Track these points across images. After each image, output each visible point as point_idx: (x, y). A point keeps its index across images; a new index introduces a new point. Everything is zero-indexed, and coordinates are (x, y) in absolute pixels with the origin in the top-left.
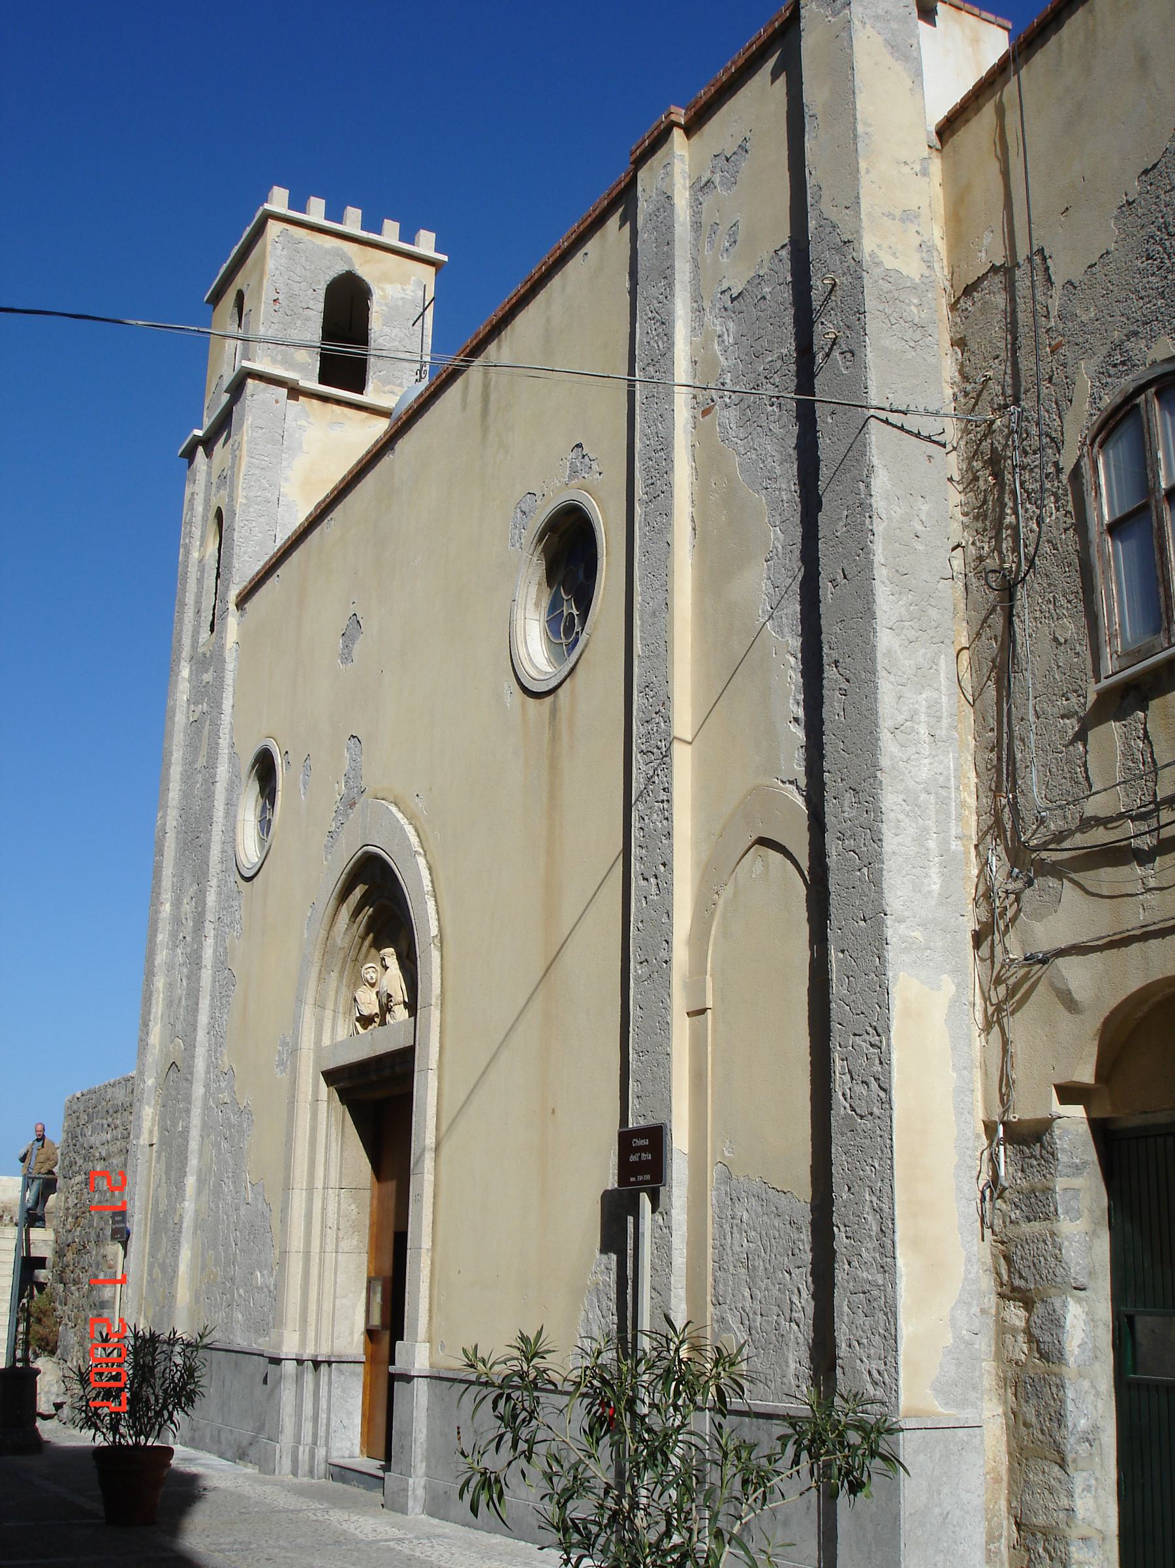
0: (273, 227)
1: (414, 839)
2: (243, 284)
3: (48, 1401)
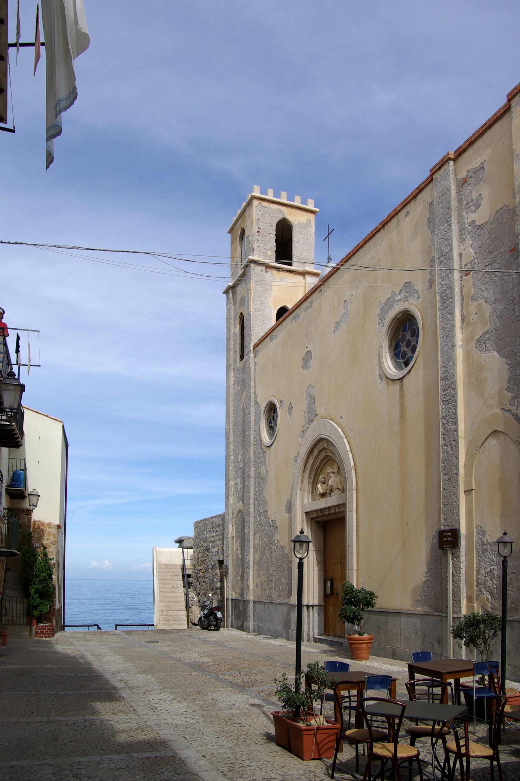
0: (256, 203)
1: (341, 433)
2: (244, 225)
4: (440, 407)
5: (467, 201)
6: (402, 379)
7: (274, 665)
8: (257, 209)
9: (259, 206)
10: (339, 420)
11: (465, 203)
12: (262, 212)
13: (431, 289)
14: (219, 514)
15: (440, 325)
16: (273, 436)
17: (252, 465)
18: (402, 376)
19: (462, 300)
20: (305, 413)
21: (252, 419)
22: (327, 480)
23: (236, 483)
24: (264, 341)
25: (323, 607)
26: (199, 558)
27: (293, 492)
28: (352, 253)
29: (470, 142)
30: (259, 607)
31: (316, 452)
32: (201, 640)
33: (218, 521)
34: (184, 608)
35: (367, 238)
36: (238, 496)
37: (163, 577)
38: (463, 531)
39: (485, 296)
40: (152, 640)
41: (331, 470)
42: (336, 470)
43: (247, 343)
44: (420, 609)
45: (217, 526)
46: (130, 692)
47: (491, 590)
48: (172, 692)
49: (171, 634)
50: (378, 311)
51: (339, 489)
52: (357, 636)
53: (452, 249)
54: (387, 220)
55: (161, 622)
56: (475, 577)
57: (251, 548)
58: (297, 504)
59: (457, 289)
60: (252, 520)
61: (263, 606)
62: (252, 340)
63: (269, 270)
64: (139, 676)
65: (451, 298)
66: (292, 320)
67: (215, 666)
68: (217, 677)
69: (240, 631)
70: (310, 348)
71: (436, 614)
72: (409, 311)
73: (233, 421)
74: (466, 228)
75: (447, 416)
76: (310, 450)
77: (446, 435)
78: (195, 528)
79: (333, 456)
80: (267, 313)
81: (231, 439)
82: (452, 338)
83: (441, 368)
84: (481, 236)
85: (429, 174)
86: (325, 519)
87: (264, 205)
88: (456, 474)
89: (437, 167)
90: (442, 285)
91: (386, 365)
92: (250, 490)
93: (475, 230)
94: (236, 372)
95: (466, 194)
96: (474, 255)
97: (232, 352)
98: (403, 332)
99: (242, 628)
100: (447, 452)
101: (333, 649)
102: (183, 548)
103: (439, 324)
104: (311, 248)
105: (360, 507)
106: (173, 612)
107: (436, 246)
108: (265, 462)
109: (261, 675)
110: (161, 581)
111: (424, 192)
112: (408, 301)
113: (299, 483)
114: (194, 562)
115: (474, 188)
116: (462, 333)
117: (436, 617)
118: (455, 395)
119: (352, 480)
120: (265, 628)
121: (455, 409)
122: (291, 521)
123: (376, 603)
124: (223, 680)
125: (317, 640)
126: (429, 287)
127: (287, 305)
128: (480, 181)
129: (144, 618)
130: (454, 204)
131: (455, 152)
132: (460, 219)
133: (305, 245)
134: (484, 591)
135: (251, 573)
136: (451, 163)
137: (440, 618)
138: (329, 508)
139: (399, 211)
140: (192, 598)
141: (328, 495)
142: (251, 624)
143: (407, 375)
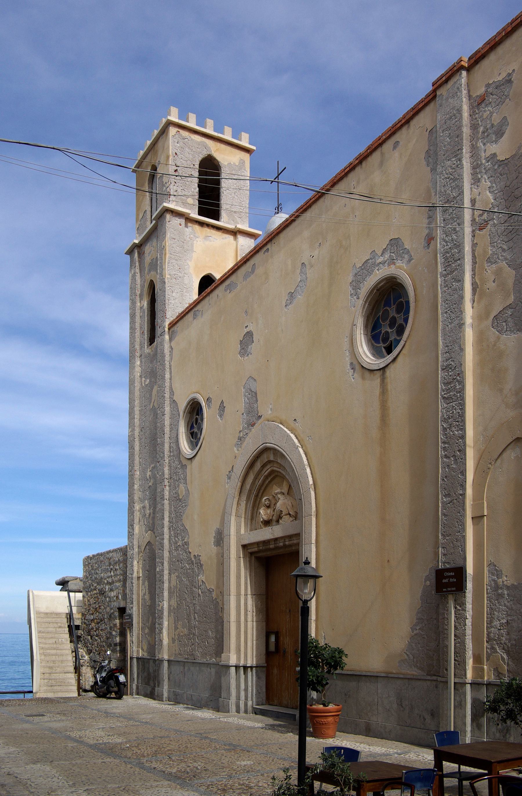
0: (172, 131)
1: (296, 441)
3: (89, 684)
4: (440, 406)
5: (485, 127)
6: (384, 369)
7: (213, 746)
8: (175, 140)
9: (177, 136)
10: (292, 424)
11: (481, 129)
12: (181, 144)
13: (428, 248)
14: (118, 547)
15: (442, 297)
16: (197, 446)
17: (166, 482)
18: (384, 365)
19: (474, 263)
20: (243, 414)
21: (167, 422)
22: (273, 502)
23: (144, 507)
24: (184, 318)
25: (265, 669)
26: (90, 605)
27: (226, 518)
28: (313, 199)
29: (493, 43)
30: (177, 669)
31: (258, 465)
32: (101, 712)
33: (117, 557)
34: (72, 669)
35: (337, 179)
36: (146, 524)
37: (43, 630)
38: (470, 570)
39: (508, 257)
40: (35, 714)
41: (278, 490)
42: (285, 490)
43: (159, 321)
44: (414, 672)
45: (116, 563)
46: (27, 792)
47: (508, 647)
48: (87, 790)
49: (57, 704)
50: (350, 278)
51: (290, 514)
52: (321, 706)
53: (463, 192)
54: (366, 154)
55: (41, 689)
56: (485, 631)
57: (165, 591)
58: (231, 534)
59: (467, 248)
60: (166, 554)
61: (182, 668)
62: (168, 316)
63: (189, 224)
64: (32, 766)
65: (459, 259)
66: (226, 290)
67: (133, 749)
68: (141, 766)
69: (150, 699)
70: (251, 328)
71: (429, 678)
72: (395, 278)
73: (140, 425)
74: (482, 164)
75: (450, 418)
76: (250, 463)
77: (448, 443)
78: (85, 565)
79: (282, 472)
80: (186, 282)
81: (137, 448)
82: (459, 313)
83: (443, 354)
84: (505, 176)
85: (431, 88)
86: (269, 554)
87: (183, 135)
88: (461, 495)
89: (444, 78)
90: (446, 242)
91: (361, 350)
92: (163, 516)
93: (496, 167)
94: (143, 360)
95: (485, 117)
96: (493, 201)
97: (138, 334)
98: (384, 306)
99: (152, 695)
100: (448, 466)
101: (282, 723)
102: (69, 591)
103: (440, 295)
104: (245, 199)
105: (321, 538)
106: (58, 674)
107: (438, 189)
108: (185, 479)
109: (201, 761)
110: (41, 634)
111: (422, 115)
112: (394, 264)
113: (233, 506)
114: (83, 610)
115: (496, 110)
116: (473, 308)
117: (429, 683)
118: (462, 390)
119: (311, 503)
120: (185, 695)
121: (460, 409)
122: (222, 556)
123: (346, 664)
124: (151, 769)
125: (256, 712)
126: (426, 245)
127: (212, 273)
128: (505, 99)
129: (22, 684)
130: (466, 131)
131: (470, 59)
132: (473, 152)
133: (236, 194)
134: (498, 649)
135: (166, 624)
136: (464, 73)
137: (434, 683)
138: (276, 540)
139: (384, 141)
140: (82, 657)
141: (274, 523)
142: (165, 690)
143: (391, 364)
